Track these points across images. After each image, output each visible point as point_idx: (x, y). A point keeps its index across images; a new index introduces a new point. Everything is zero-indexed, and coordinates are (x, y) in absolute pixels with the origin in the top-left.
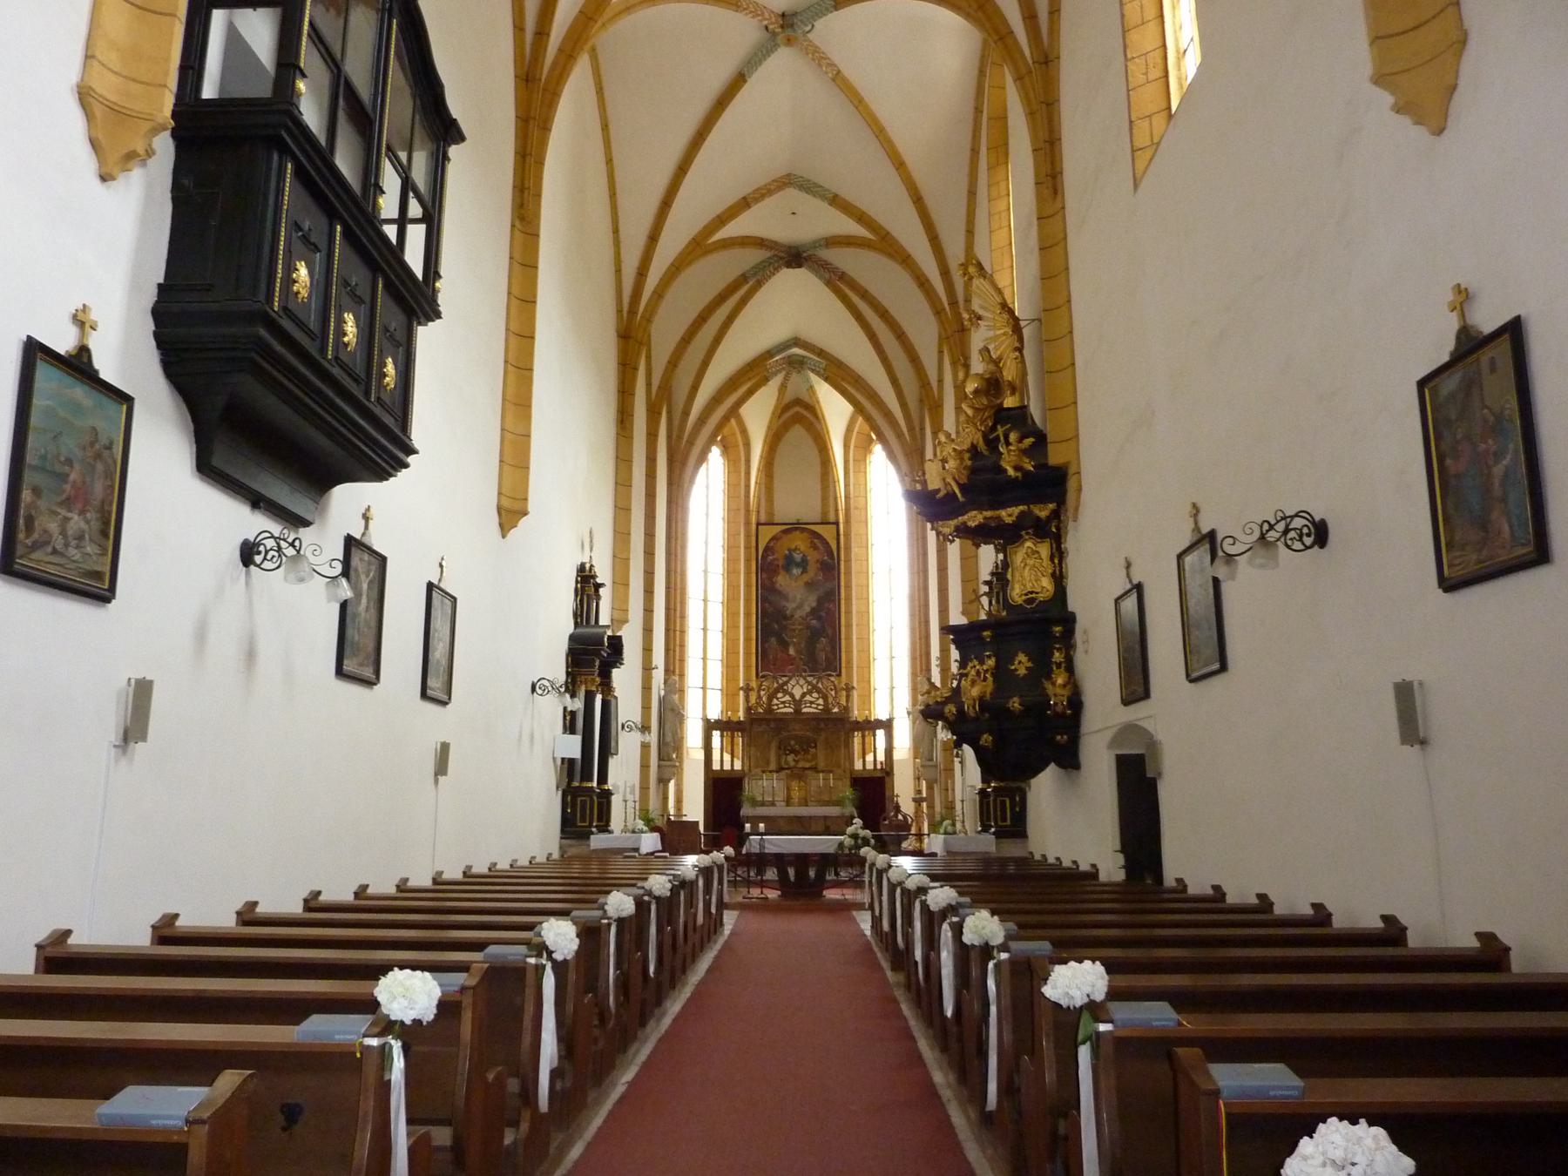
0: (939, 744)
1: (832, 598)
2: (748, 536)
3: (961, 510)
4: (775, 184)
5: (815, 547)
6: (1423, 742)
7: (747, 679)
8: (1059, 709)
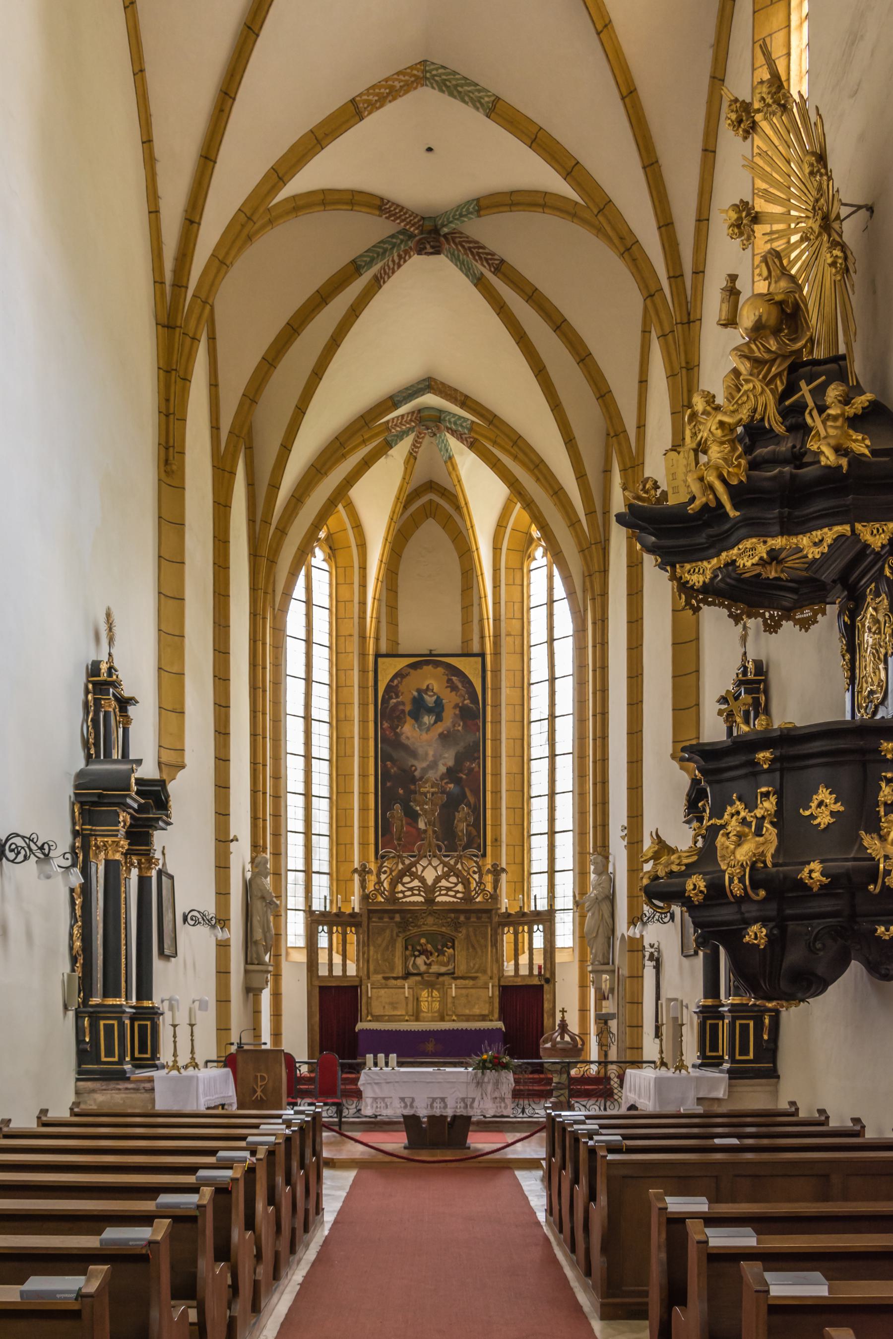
0: (618, 943)
1: (476, 755)
2: (363, 671)
4: (401, 77)
5: (453, 688)
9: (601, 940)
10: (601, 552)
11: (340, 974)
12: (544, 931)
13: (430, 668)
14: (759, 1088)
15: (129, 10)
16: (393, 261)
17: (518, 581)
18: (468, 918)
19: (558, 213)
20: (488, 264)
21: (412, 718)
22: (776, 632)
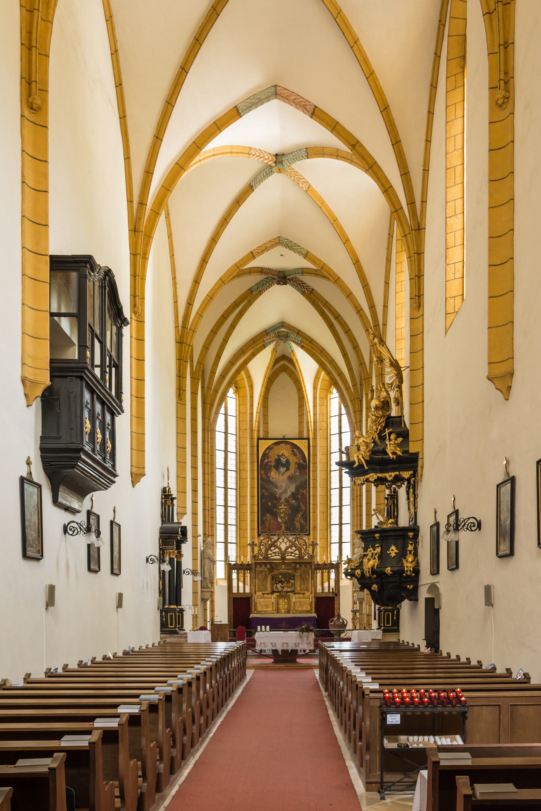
1: (305, 487)
2: (252, 446)
3: (365, 473)
4: (270, 243)
5: (295, 454)
6: (492, 605)
7: (252, 537)
8: (409, 573)
10: (359, 402)
12: (335, 572)
13: (283, 445)
15: (170, 238)
17: (325, 404)
18: (301, 566)
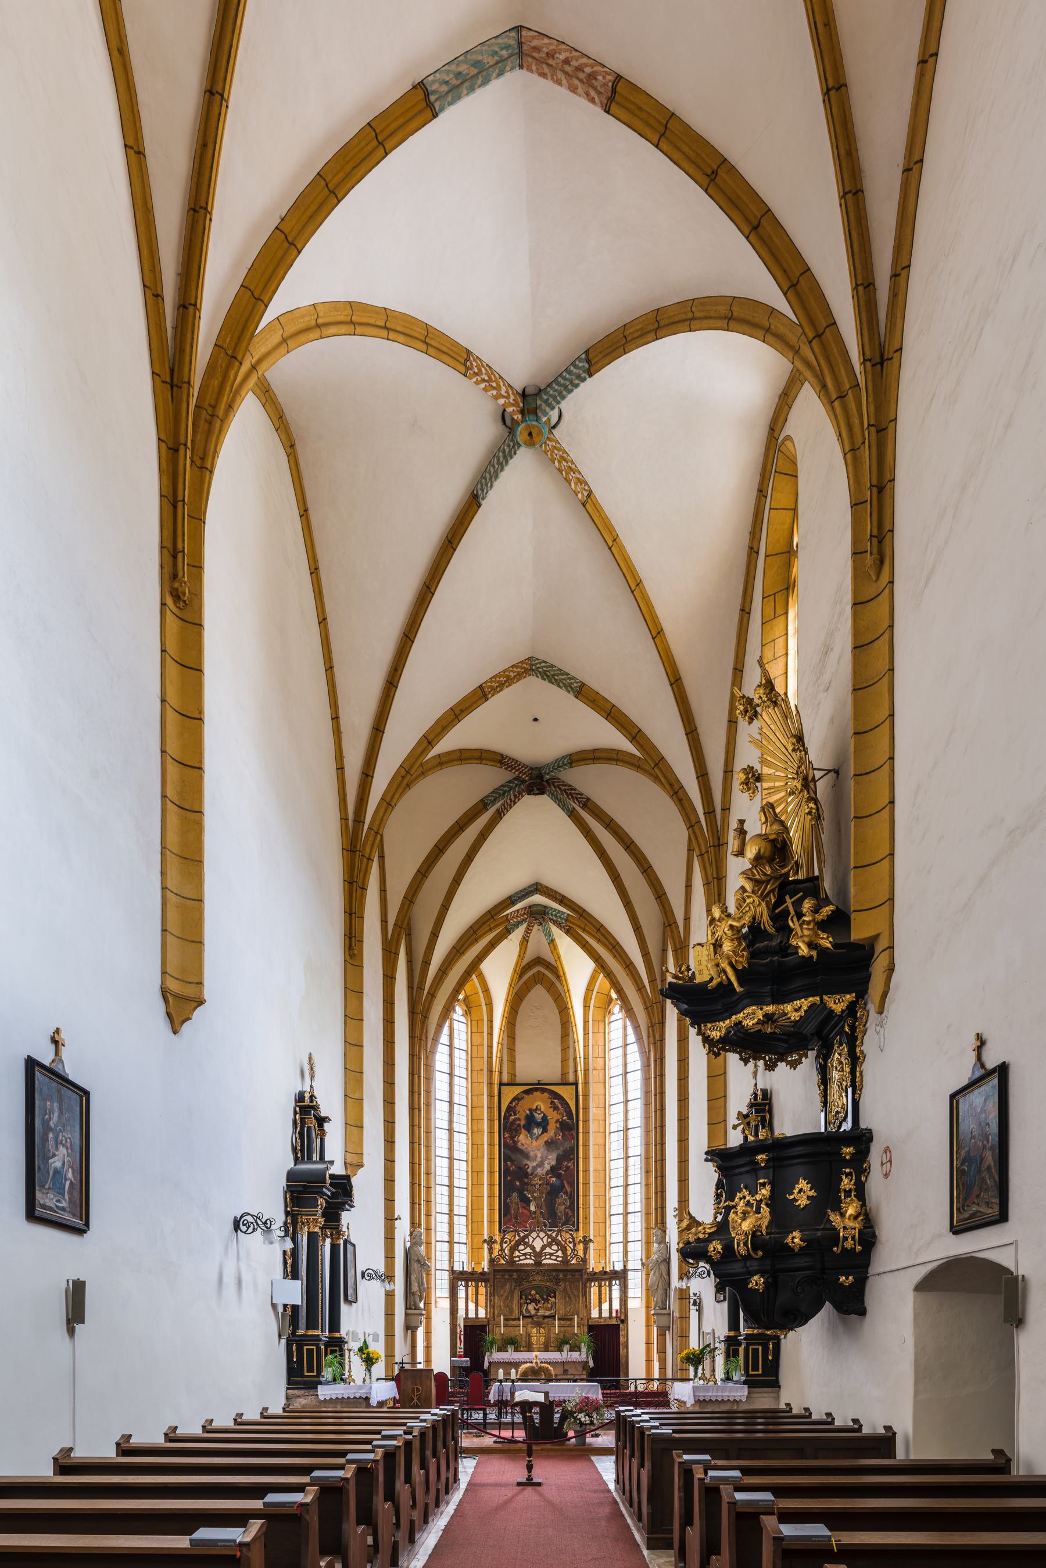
0: (672, 1294)
1: (571, 1157)
2: (490, 1096)
4: (515, 669)
5: (555, 1108)
8: (849, 1244)
9: (660, 1291)
11: (474, 1316)
12: (620, 1285)
14: (766, 1395)
16: (510, 799)
19: (626, 766)
20: (578, 801)
21: (526, 1130)
22: (774, 1070)
